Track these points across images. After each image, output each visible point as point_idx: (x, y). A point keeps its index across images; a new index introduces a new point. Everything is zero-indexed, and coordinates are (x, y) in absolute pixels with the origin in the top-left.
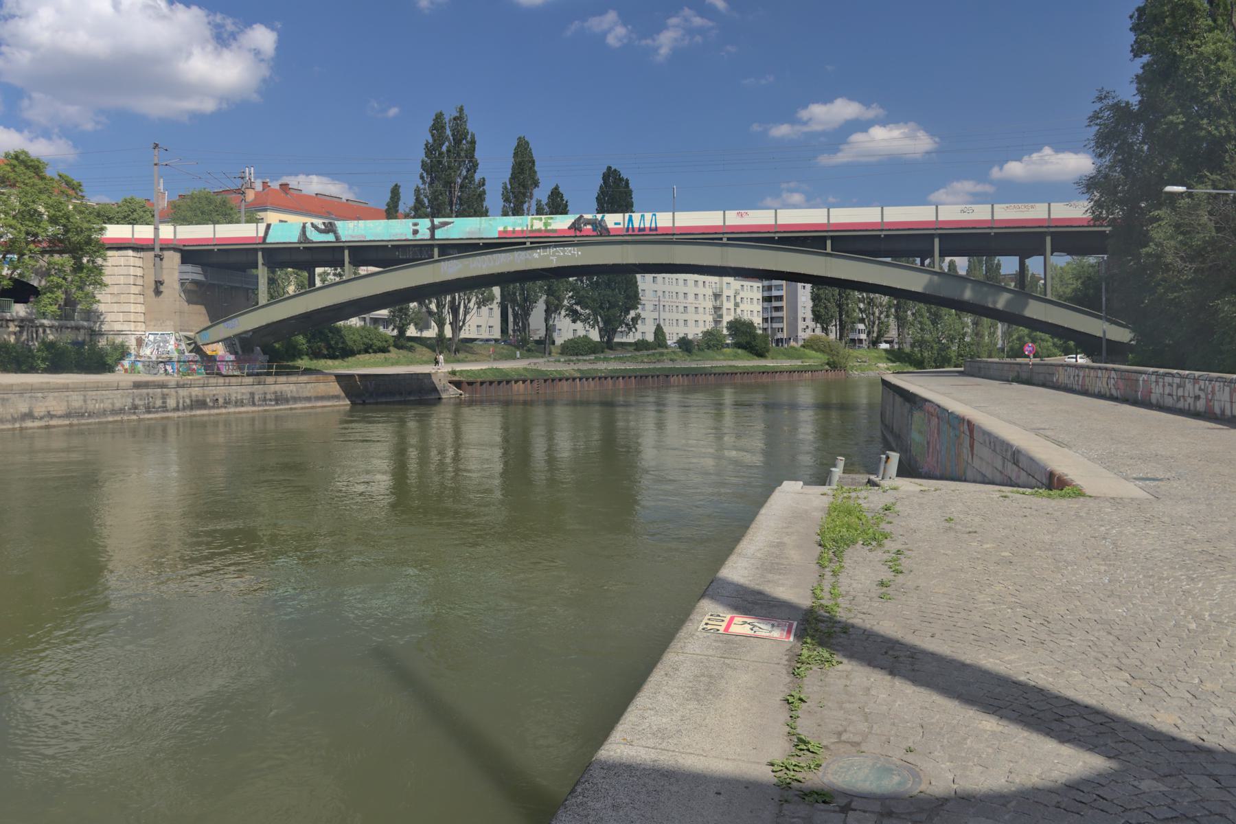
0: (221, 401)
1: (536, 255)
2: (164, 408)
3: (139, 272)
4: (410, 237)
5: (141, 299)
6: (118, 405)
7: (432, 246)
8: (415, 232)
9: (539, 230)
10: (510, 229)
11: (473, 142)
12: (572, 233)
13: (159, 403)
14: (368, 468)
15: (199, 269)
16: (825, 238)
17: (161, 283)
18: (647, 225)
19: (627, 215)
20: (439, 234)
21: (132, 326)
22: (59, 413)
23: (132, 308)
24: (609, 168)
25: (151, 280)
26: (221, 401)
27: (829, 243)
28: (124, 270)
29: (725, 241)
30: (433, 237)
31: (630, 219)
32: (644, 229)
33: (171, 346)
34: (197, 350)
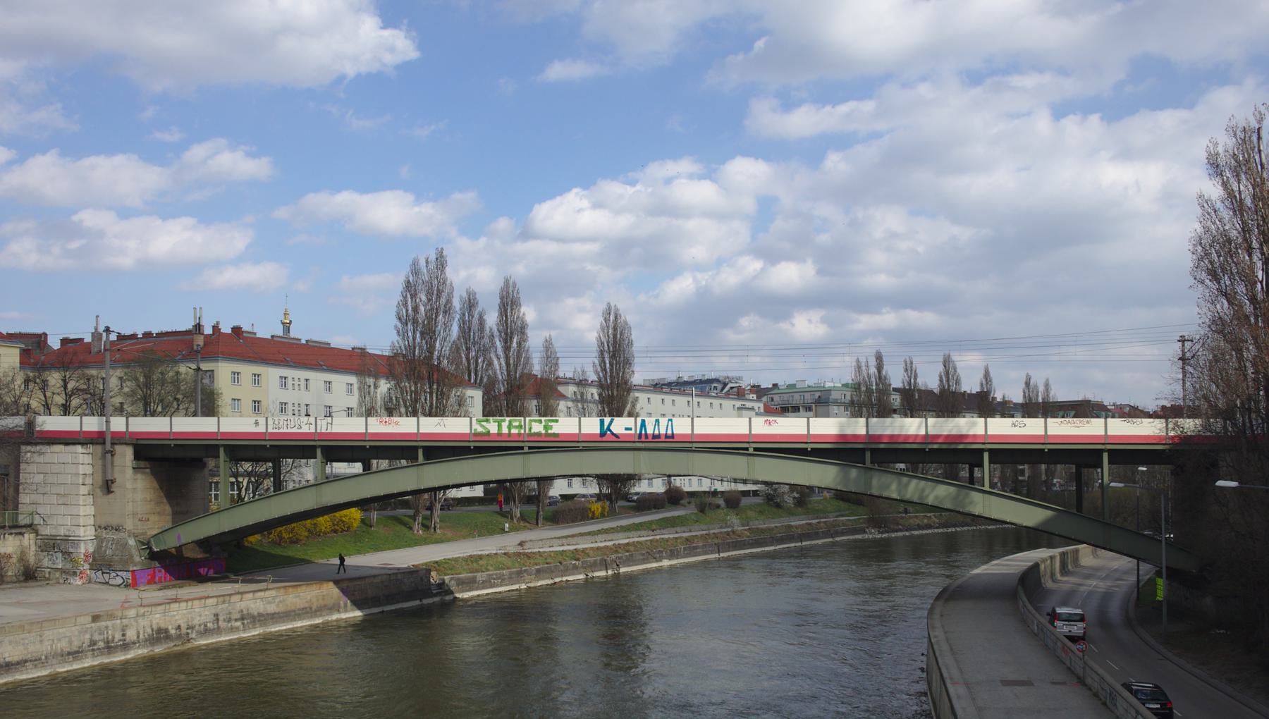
9: (539, 434)
16: (416, 448)
17: (113, 482)
18: (663, 431)
25: (99, 481)
27: (420, 452)
29: (751, 451)
32: (659, 436)
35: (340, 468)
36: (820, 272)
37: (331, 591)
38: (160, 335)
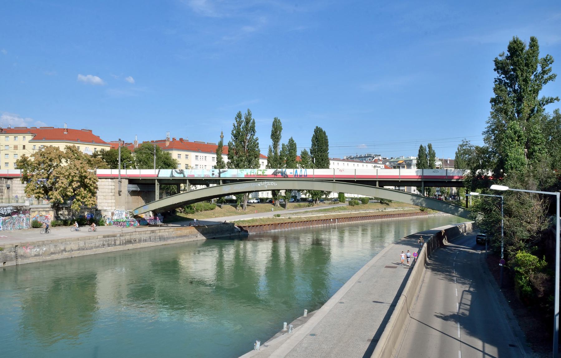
0: (137, 240)
1: (259, 185)
2: (115, 245)
3: (113, 187)
4: (211, 176)
5: (114, 197)
6: (97, 245)
7: (219, 180)
8: (213, 174)
9: (260, 175)
10: (249, 174)
11: (254, 123)
12: (273, 176)
13: (113, 243)
14: (203, 264)
15: (136, 186)
16: (376, 181)
17: (121, 191)
18: (303, 174)
19: (295, 170)
20: (222, 175)
21: (110, 208)
22: (76, 249)
23: (110, 201)
24: (317, 127)
25: (117, 190)
26: (137, 240)
27: (377, 183)
28: (107, 187)
29: (334, 181)
30: (219, 177)
31: (296, 171)
32: (301, 176)
33: (124, 216)
34: (136, 217)
35: (199, 187)
36: (545, 118)
37: (194, 230)
38: (157, 141)
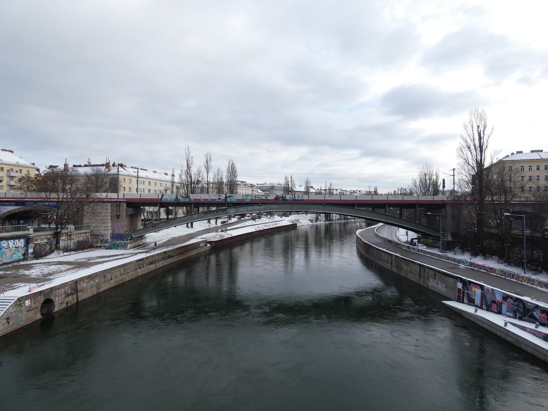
9: (264, 199)
